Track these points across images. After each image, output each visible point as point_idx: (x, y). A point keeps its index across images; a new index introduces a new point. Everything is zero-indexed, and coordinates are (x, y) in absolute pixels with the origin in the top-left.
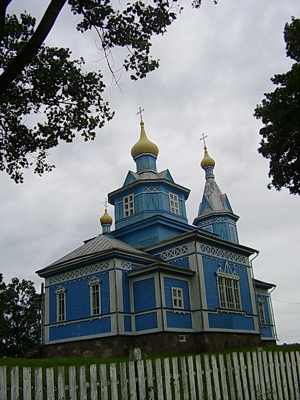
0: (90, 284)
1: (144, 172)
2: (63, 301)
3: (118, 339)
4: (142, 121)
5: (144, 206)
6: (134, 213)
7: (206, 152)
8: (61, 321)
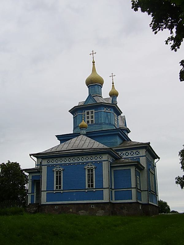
0: (86, 168)
1: (96, 96)
2: (60, 176)
3: (110, 205)
4: (93, 60)
5: (102, 119)
6: (94, 123)
7: (113, 86)
8: (57, 189)
